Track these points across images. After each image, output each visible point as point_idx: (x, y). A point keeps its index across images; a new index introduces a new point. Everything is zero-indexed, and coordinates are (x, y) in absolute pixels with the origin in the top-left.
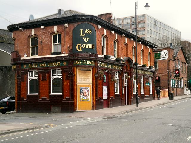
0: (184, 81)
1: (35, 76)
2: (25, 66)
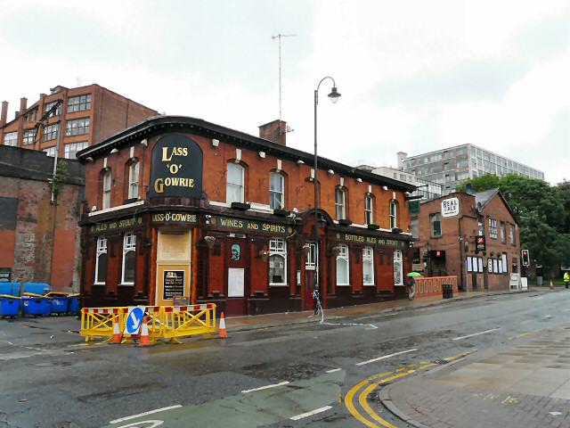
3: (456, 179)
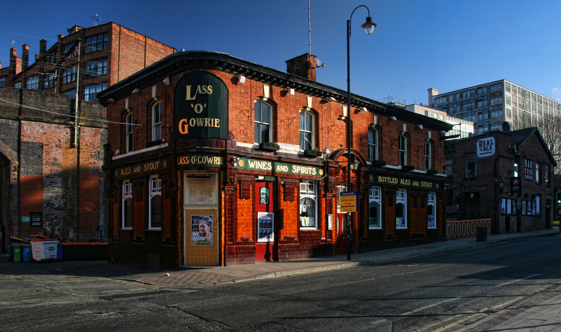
0: (544, 202)
3: (489, 117)
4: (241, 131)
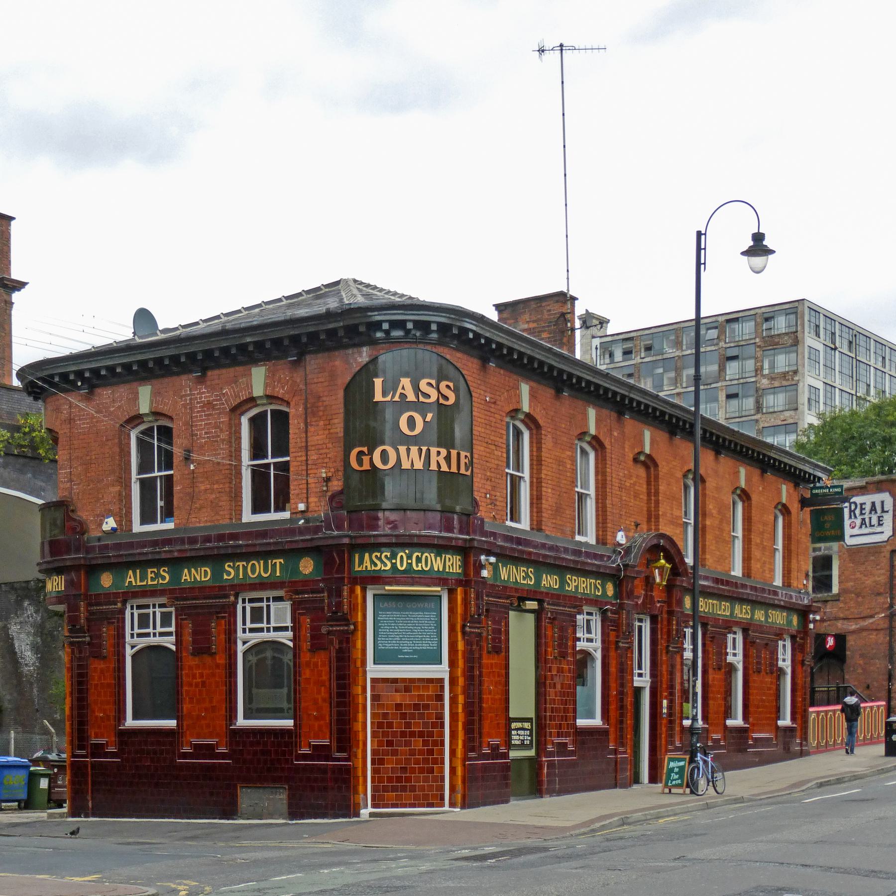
1: (159, 629)
2: (106, 580)
3: (759, 408)
4: (486, 494)
